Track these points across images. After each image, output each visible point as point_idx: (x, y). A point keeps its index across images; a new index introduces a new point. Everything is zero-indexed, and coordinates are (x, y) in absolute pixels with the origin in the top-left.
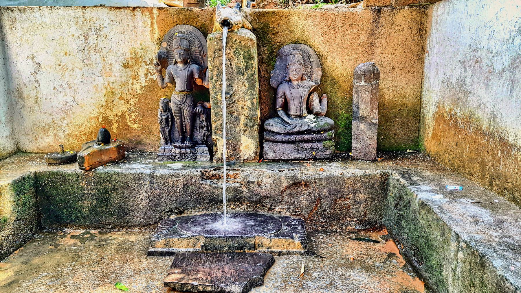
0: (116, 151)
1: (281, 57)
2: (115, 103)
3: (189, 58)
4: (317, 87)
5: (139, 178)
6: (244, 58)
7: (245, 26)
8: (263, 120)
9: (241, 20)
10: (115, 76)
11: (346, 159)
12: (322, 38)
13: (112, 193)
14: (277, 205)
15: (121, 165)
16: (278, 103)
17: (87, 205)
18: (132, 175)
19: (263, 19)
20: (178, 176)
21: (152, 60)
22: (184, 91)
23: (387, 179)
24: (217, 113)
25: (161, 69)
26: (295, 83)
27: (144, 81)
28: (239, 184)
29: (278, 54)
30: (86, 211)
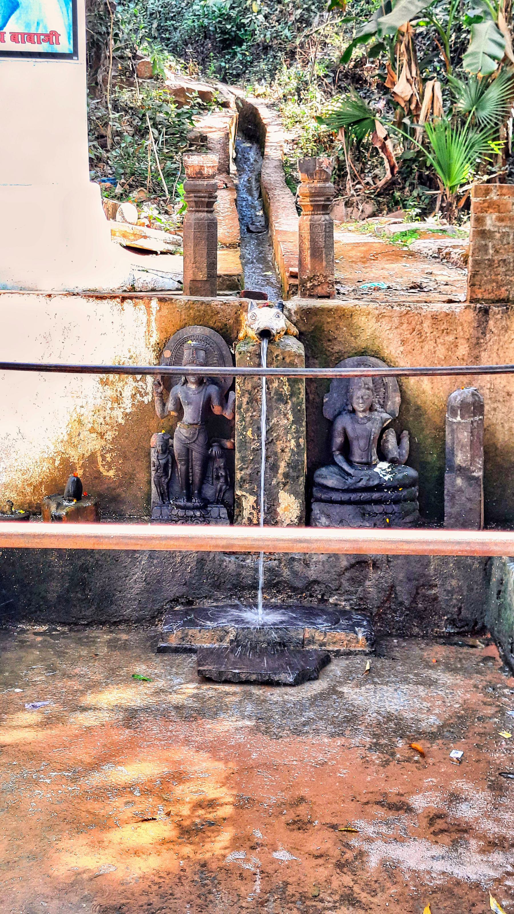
2: (81, 436)
4: (394, 420)
8: (313, 467)
12: (402, 349)
14: (331, 595)
17: (54, 589)
19: (315, 319)
24: (245, 457)
27: (130, 405)
30: (52, 596)
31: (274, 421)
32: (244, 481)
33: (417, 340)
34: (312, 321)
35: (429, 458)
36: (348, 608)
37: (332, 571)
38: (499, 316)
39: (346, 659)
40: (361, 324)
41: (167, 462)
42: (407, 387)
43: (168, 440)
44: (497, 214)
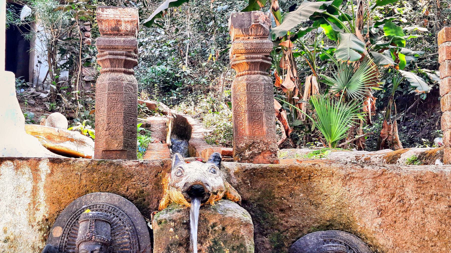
9: (223, 185)
12: (379, 220)
19: (261, 183)
33: (398, 209)
40: (324, 188)
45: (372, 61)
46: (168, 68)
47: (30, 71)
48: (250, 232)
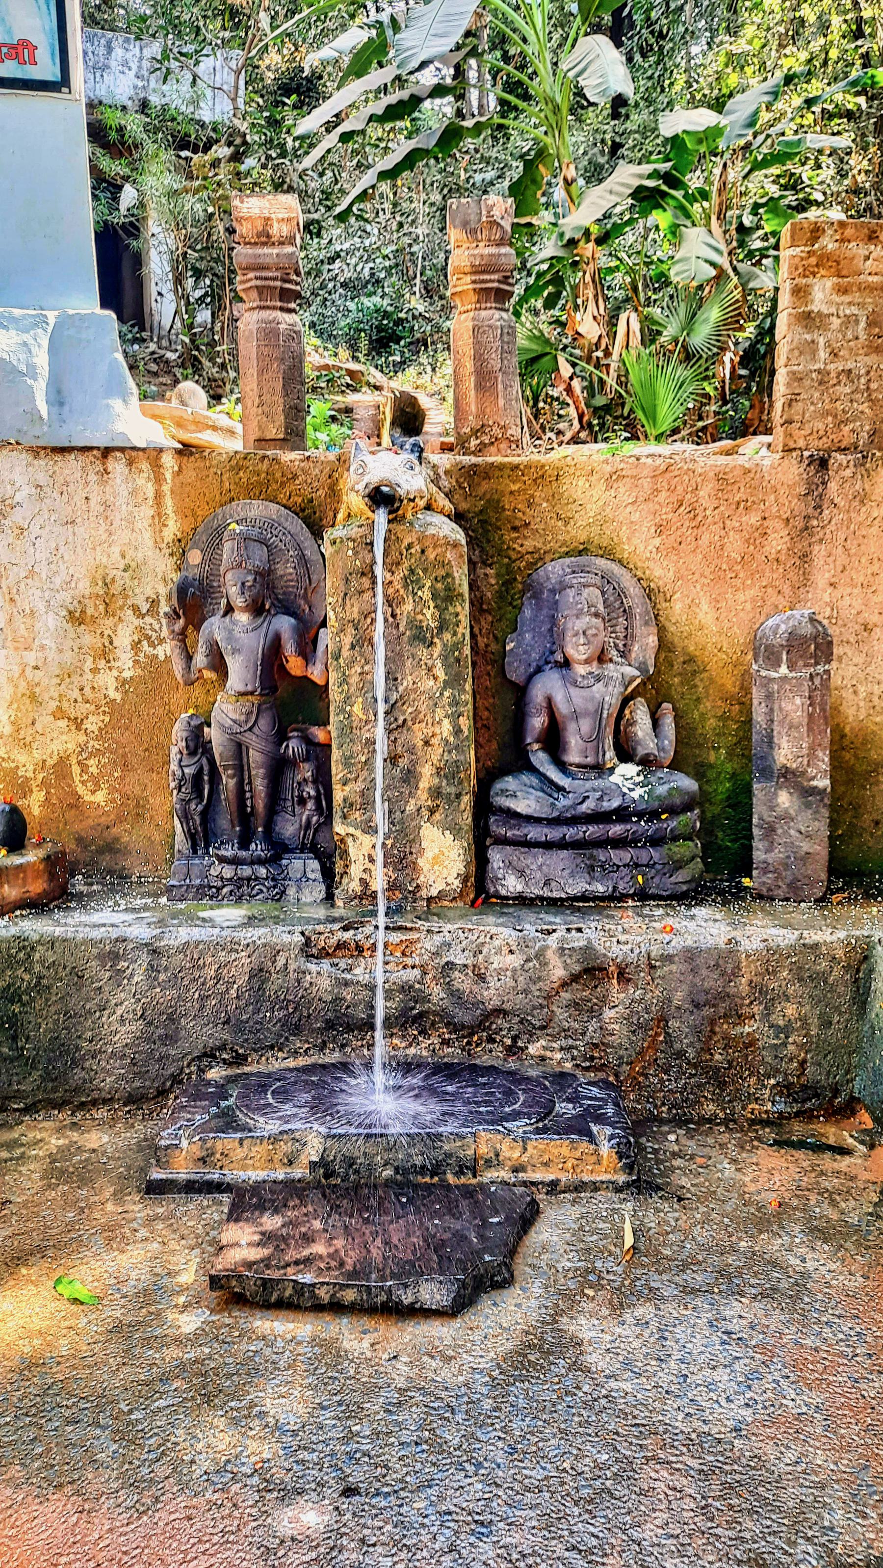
0: (44, 871)
1: (537, 596)
2: (39, 726)
3: (268, 597)
5: (113, 954)
6: (434, 597)
7: (434, 506)
8: (487, 779)
9: (424, 488)
10: (43, 647)
11: (737, 897)
12: (657, 541)
13: (33, 1000)
14: (532, 1037)
15: (58, 915)
16: (529, 727)
18: (93, 943)
19: (485, 486)
20: (232, 946)
21: (154, 603)
22: (252, 693)
23: (866, 958)
24: (351, 757)
25: (185, 629)
26: (581, 670)
27: (131, 664)
28: (417, 972)
29: (527, 587)
31: (407, 682)
32: (351, 805)
34: (481, 491)
35: (712, 757)
36: (568, 1065)
37: (534, 988)
38: (848, 473)
39: (574, 1202)
41: (200, 770)
42: (667, 619)
43: (200, 728)
44: (835, 280)
45: (735, 280)
46: (386, 301)
47: (146, 310)
48: (461, 556)
